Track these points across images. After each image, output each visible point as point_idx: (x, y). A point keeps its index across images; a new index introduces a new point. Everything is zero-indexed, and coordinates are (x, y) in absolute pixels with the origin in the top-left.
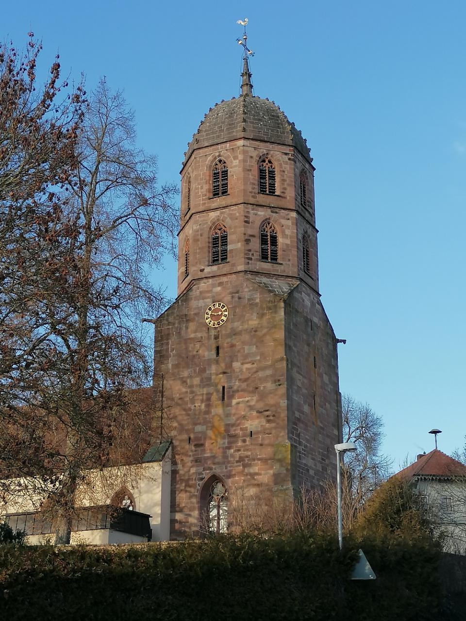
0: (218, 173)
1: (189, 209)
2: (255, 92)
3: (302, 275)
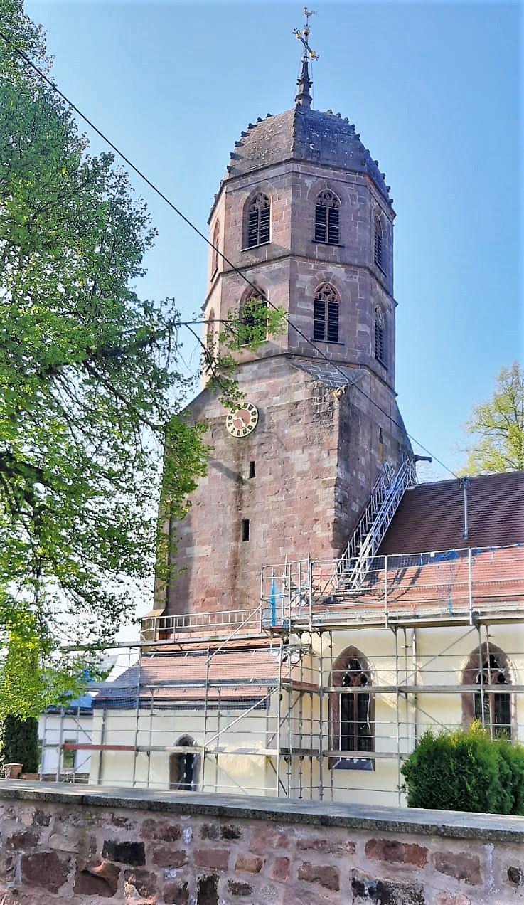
0: (257, 214)
1: (217, 269)
2: (313, 106)
3: (372, 266)
